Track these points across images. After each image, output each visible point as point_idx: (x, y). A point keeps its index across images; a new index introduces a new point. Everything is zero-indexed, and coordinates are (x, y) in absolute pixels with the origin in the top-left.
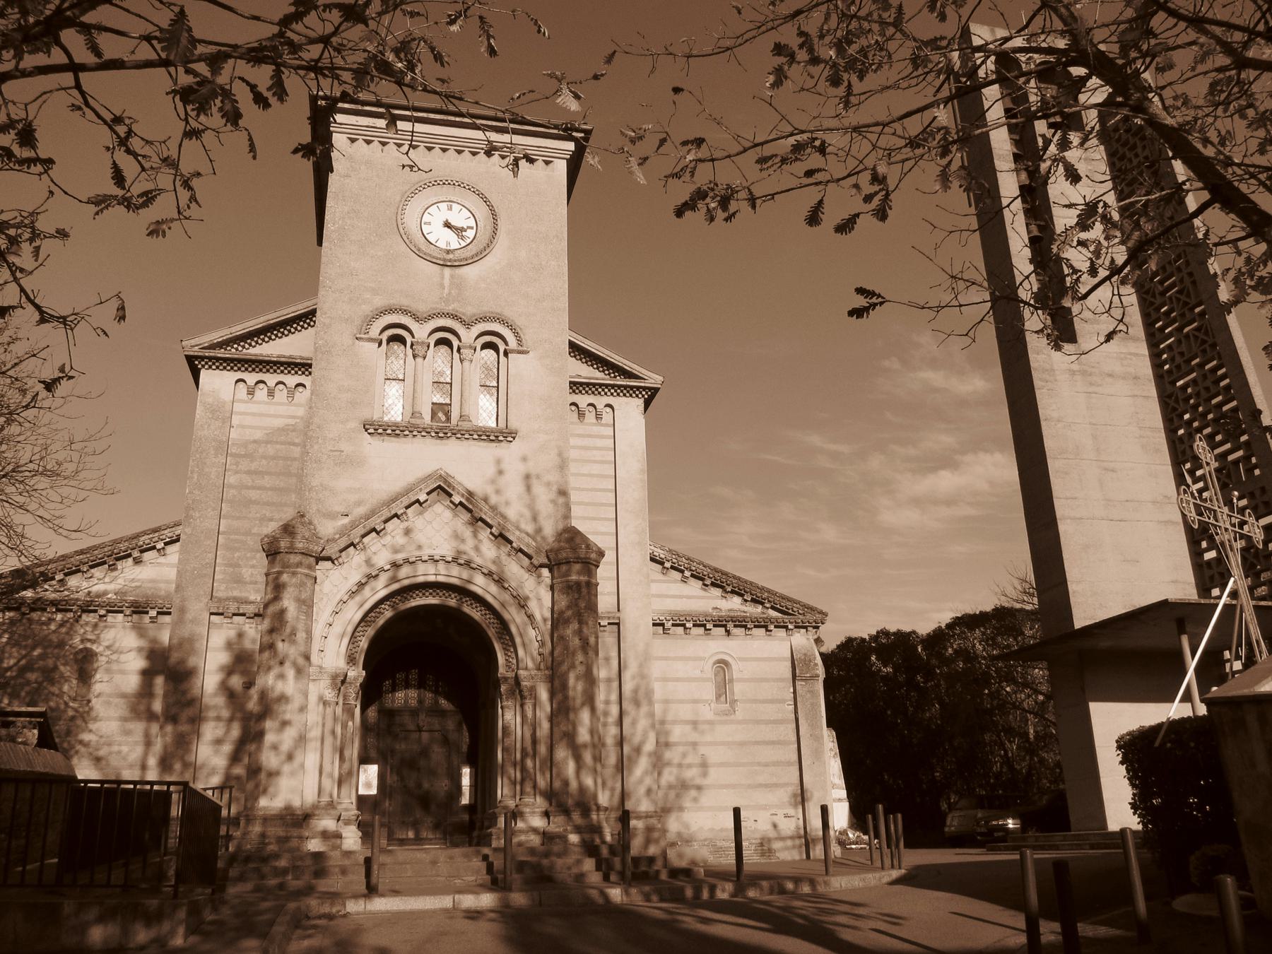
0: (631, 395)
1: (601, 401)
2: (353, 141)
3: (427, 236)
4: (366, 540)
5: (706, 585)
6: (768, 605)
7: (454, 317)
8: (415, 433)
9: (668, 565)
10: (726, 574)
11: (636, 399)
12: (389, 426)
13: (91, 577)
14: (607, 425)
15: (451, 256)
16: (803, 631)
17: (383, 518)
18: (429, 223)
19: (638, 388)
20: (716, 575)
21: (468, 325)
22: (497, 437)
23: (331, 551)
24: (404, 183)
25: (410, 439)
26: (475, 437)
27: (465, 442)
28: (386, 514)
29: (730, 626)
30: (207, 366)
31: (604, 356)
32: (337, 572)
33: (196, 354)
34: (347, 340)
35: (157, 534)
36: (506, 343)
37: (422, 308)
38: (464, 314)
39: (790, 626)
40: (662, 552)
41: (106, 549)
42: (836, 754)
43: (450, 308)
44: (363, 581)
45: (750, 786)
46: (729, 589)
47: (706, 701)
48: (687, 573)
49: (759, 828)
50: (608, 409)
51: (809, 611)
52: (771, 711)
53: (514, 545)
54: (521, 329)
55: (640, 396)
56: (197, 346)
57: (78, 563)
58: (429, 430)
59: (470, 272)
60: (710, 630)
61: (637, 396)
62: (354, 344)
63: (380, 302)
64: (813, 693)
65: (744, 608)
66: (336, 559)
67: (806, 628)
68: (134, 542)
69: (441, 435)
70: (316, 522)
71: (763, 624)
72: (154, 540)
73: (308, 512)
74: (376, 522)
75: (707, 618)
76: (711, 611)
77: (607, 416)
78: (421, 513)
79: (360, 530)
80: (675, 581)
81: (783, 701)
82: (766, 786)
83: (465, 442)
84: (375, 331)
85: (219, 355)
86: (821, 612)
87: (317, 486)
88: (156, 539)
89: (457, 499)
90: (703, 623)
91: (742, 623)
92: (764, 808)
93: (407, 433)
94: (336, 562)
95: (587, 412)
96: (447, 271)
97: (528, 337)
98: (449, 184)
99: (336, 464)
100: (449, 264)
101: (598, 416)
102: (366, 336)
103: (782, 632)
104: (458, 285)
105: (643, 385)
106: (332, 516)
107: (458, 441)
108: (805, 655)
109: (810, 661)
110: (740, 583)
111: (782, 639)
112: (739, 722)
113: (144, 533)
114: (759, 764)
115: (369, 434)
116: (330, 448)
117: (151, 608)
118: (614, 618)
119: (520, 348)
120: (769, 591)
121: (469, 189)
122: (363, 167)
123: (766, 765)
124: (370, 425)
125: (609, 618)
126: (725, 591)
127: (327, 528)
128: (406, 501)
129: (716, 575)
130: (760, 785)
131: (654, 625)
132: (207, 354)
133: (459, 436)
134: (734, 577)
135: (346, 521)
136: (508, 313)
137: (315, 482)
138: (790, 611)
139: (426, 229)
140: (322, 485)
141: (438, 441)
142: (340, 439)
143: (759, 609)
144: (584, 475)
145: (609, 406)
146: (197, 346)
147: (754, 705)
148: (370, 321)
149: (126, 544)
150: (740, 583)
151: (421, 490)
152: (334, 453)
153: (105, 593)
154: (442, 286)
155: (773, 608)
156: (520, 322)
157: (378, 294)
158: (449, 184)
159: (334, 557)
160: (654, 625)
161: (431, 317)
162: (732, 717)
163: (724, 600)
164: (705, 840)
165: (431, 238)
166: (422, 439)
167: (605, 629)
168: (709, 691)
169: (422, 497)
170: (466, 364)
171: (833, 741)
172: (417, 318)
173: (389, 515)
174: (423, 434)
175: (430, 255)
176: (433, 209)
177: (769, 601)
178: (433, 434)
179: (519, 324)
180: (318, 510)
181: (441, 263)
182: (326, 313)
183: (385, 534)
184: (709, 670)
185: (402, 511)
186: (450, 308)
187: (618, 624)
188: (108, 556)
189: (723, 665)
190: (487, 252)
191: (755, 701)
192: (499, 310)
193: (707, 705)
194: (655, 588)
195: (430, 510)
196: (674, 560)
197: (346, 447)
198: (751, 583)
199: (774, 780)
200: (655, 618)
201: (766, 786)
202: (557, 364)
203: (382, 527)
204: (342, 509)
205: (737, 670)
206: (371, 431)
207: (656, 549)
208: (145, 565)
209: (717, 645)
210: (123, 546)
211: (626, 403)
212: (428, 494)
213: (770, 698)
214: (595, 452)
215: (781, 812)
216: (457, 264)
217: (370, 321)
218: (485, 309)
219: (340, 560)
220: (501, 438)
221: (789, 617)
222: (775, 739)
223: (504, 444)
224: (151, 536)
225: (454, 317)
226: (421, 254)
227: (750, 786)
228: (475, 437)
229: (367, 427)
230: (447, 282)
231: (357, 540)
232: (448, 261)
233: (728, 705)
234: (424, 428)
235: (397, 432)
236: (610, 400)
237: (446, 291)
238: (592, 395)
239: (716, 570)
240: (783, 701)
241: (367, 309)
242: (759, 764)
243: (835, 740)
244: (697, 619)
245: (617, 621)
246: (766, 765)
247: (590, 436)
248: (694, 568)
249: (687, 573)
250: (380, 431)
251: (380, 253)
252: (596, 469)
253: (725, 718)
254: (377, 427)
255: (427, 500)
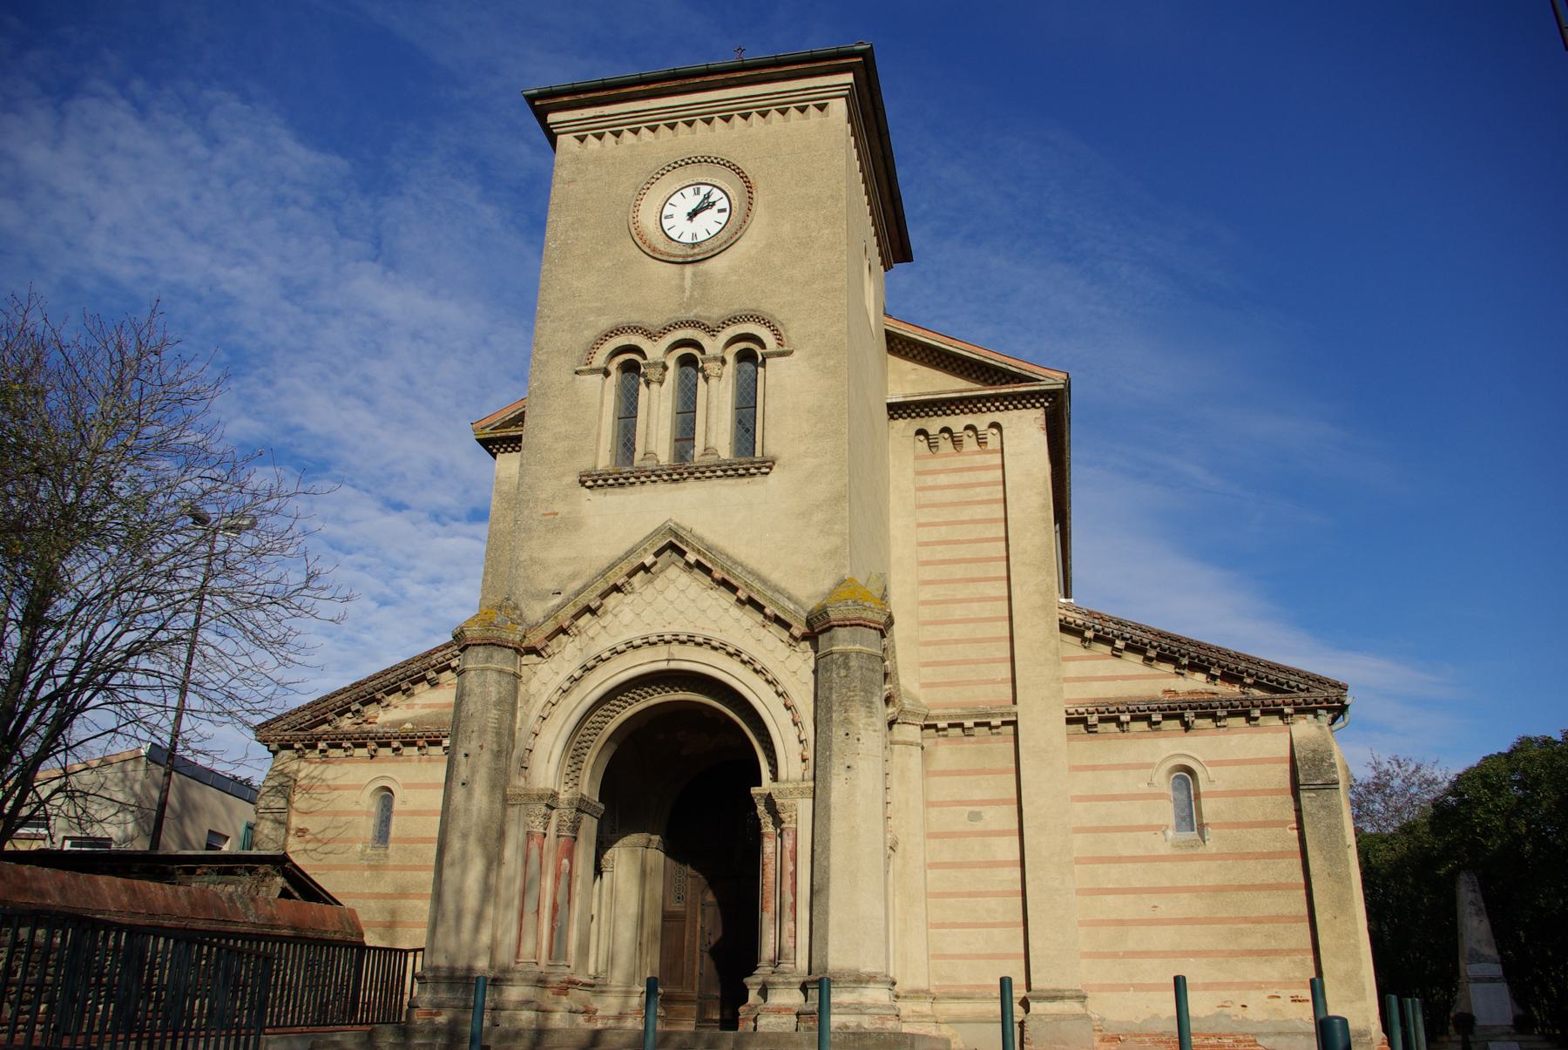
0: (1025, 407)
1: (982, 421)
2: (582, 139)
3: (668, 232)
4: (582, 622)
5: (1151, 659)
6: (1249, 681)
7: (695, 324)
8: (643, 479)
9: (1089, 634)
10: (1178, 640)
11: (1033, 411)
12: (610, 474)
13: (388, 705)
14: (993, 452)
15: (696, 251)
16: (1310, 717)
17: (599, 592)
18: (671, 216)
19: (1032, 394)
20: (1163, 642)
21: (712, 332)
22: (747, 469)
23: (535, 639)
24: (637, 173)
25: (638, 487)
26: (719, 473)
27: (708, 482)
28: (602, 586)
29: (1189, 715)
30: (502, 450)
31: (981, 358)
32: (546, 666)
33: (487, 436)
34: (567, 376)
35: (449, 650)
36: (763, 346)
37: (656, 321)
38: (709, 319)
39: (1287, 710)
40: (1078, 616)
41: (398, 672)
42: (1480, 909)
43: (691, 315)
44: (576, 675)
45: (1232, 954)
46: (1185, 661)
47: (1158, 828)
48: (1120, 644)
49: (1250, 1017)
50: (995, 431)
51: (1315, 684)
52: (1261, 840)
53: (767, 611)
54: (782, 324)
55: (1038, 405)
56: (488, 426)
57: (371, 690)
58: (659, 472)
59: (717, 265)
60: (1159, 723)
61: (1034, 406)
62: (574, 379)
63: (605, 323)
64: (1334, 812)
65: (1211, 687)
66: (542, 649)
67: (1314, 712)
68: (428, 660)
69: (675, 477)
70: (522, 605)
71: (1241, 711)
72: (447, 657)
73: (514, 594)
74: (591, 598)
75: (1152, 706)
76: (1160, 695)
77: (993, 439)
78: (651, 581)
79: (571, 610)
80: (1104, 657)
81: (1283, 824)
82: (1259, 953)
83: (708, 481)
84: (599, 360)
85: (511, 434)
86: (1336, 685)
87: (525, 561)
88: (450, 655)
89: (691, 557)
90: (1148, 715)
91: (1208, 710)
92: (1258, 986)
93: (632, 480)
94: (543, 653)
95: (965, 438)
96: (689, 269)
97: (792, 334)
98: (694, 162)
99: (548, 531)
100: (690, 259)
101: (981, 441)
102: (588, 367)
103: (1275, 721)
104: (702, 283)
105: (1037, 388)
106: (541, 596)
107: (699, 483)
108: (1314, 751)
109: (1322, 760)
110: (1201, 651)
111: (1278, 730)
112: (1212, 857)
113: (437, 650)
114: (1246, 920)
115: (589, 487)
116: (543, 511)
117: (444, 737)
118: (1009, 714)
119: (781, 349)
120: (1248, 660)
121: (718, 163)
122: (591, 167)
123: (1258, 921)
124: (588, 476)
125: (1002, 715)
126: (1178, 665)
127: (535, 611)
128: (627, 567)
129: (1163, 642)
130: (1250, 953)
131: (1069, 721)
132: (498, 435)
133: (698, 475)
134: (1191, 643)
135: (557, 600)
136: (767, 307)
137: (524, 556)
138: (1285, 687)
139: (667, 224)
140: (531, 559)
141: (674, 485)
142: (554, 498)
143: (1237, 688)
144: (963, 522)
145: (995, 425)
146: (488, 426)
147: (1235, 831)
148: (592, 350)
149: (419, 664)
150: (1201, 651)
151: (645, 550)
152: (547, 517)
153: (401, 723)
154: (682, 289)
155: (1257, 685)
156: (780, 316)
157: (604, 314)
158: (694, 162)
159: (539, 647)
160: (1069, 721)
161: (666, 330)
162: (1200, 850)
163: (1181, 678)
164: (1162, 1034)
165: (673, 234)
166: (653, 485)
167: (999, 730)
168: (1166, 813)
169: (648, 560)
170: (713, 381)
171: (1474, 891)
172: (649, 335)
173: (606, 587)
174: (653, 478)
175: (668, 254)
176: (676, 199)
177: (1250, 675)
178: (666, 477)
179: (780, 318)
180: (526, 590)
181: (680, 260)
182: (542, 348)
183: (605, 613)
184: (1163, 784)
185: (622, 580)
186: (692, 314)
187: (1015, 723)
188: (401, 680)
189: (1185, 775)
190: (739, 234)
191: (1237, 825)
192: (753, 305)
193: (1160, 833)
194: (1072, 669)
195: (661, 576)
196: (1097, 627)
197: (561, 508)
198: (1218, 650)
199: (1273, 944)
200: (1070, 711)
201: (1259, 953)
202: (832, 363)
203: (598, 603)
204: (553, 586)
205: (1207, 779)
206: (589, 483)
207: (1068, 613)
208: (443, 687)
209: (1171, 745)
210: (416, 667)
211: (1020, 417)
212: (657, 554)
213: (1260, 819)
214: (978, 490)
215: (1286, 994)
216: (699, 258)
217: (592, 350)
218: (736, 307)
219: (549, 650)
220: (752, 471)
221: (1283, 696)
222: (1272, 881)
223: (758, 478)
224: (444, 652)
225: (695, 324)
226: (655, 255)
227: (1232, 954)
228: (719, 473)
229: (584, 479)
230: (688, 283)
231: (567, 623)
232: (694, 256)
233: (1196, 832)
234: (653, 471)
235: (621, 481)
236: (969, 419)
237: (687, 294)
238: (970, 414)
239: (1160, 634)
240: (1283, 824)
241: (590, 335)
242: (1246, 920)
243: (1477, 888)
244: (1134, 708)
245: (1014, 719)
246: (1258, 921)
247: (971, 469)
248: (1128, 636)
249: (1120, 644)
250: (600, 482)
251: (607, 265)
252: (980, 512)
253: (1191, 851)
254: (596, 478)
255: (655, 563)
